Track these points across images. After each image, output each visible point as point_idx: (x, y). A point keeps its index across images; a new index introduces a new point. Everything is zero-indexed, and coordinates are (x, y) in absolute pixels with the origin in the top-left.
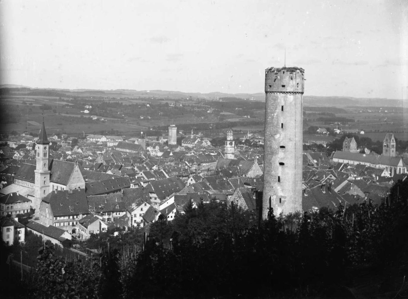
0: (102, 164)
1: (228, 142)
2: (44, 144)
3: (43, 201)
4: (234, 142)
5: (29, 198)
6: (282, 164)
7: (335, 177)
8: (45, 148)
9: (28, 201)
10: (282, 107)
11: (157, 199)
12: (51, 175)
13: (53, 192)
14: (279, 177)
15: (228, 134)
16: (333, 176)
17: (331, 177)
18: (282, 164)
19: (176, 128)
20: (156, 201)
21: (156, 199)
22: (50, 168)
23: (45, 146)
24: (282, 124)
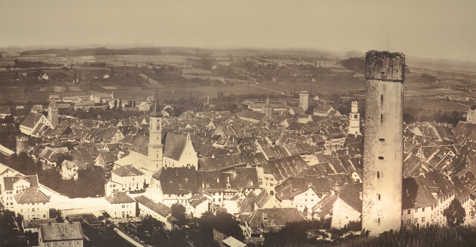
0: (220, 136)
1: (353, 115)
2: (157, 117)
3: (153, 177)
4: (358, 115)
5: (143, 171)
6: (381, 158)
7: (455, 153)
8: (158, 121)
9: (141, 174)
10: (382, 96)
11: (274, 180)
12: (164, 149)
13: (163, 168)
14: (378, 172)
15: (352, 105)
16: (452, 153)
17: (451, 153)
18: (381, 158)
19: (308, 95)
20: (272, 182)
21: (272, 180)
22: (163, 141)
23: (158, 118)
24: (382, 115)
